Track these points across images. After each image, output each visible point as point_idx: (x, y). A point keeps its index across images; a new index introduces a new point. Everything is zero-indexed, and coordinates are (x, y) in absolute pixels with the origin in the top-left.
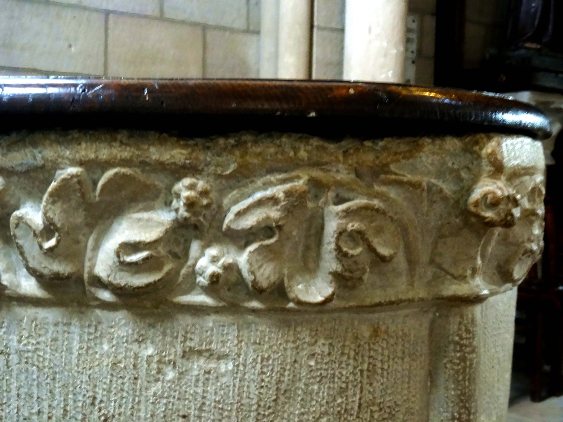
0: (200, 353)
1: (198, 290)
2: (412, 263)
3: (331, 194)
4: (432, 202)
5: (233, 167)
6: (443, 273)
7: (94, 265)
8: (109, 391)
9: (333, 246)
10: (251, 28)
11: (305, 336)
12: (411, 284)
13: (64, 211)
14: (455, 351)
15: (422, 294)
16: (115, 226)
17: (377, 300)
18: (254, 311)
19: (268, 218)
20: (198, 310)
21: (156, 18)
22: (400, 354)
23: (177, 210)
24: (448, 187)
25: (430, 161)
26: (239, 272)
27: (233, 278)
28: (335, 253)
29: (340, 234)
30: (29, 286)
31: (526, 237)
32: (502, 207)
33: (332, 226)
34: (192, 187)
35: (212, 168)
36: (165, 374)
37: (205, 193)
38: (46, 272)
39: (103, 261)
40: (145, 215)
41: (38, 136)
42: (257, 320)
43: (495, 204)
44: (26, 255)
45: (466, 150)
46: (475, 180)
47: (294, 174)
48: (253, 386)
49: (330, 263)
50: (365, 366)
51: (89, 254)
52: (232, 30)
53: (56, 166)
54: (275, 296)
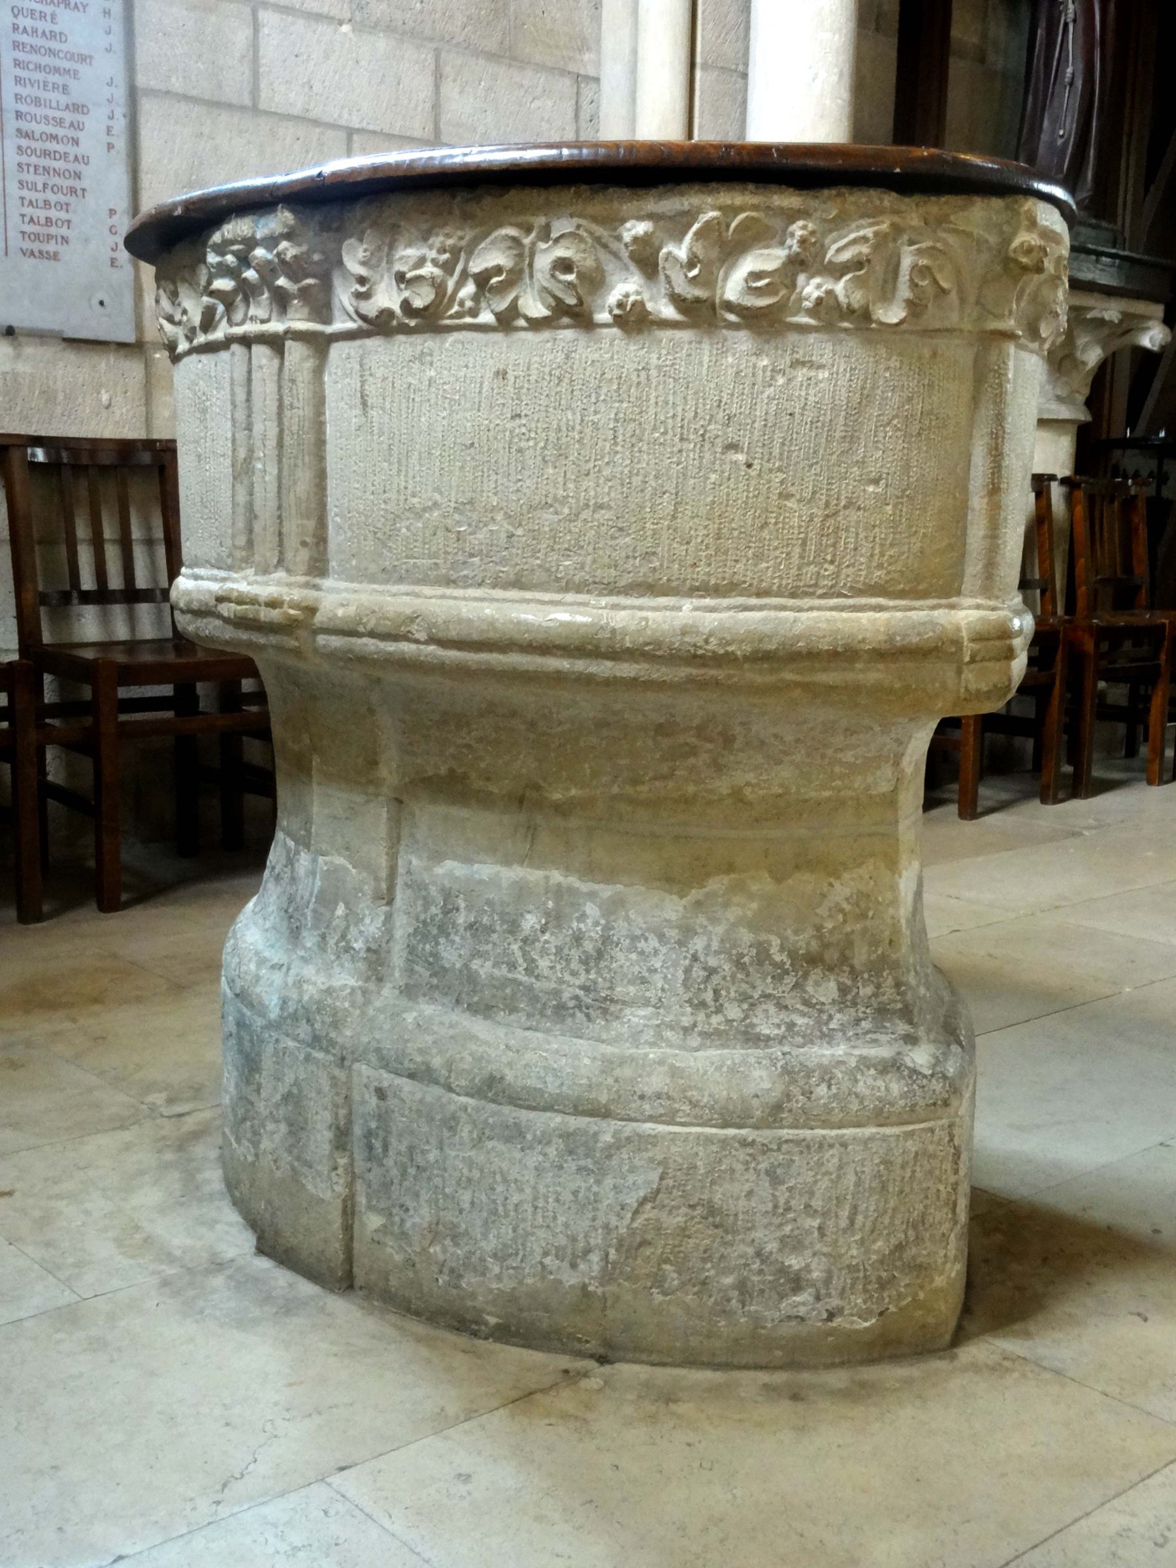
0: (803, 364)
1: (803, 313)
2: (962, 300)
3: (906, 237)
4: (979, 251)
5: (834, 213)
6: (985, 311)
7: (723, 293)
8: (732, 395)
9: (908, 277)
11: (883, 351)
12: (962, 319)
13: (704, 247)
14: (994, 377)
16: (741, 261)
18: (846, 330)
19: (860, 253)
20: (803, 329)
23: (790, 247)
24: (993, 239)
25: (978, 215)
26: (836, 297)
27: (832, 302)
28: (908, 284)
29: (913, 268)
31: (1052, 298)
32: (1035, 254)
33: (907, 262)
34: (804, 228)
35: (818, 214)
37: (813, 233)
38: (689, 296)
40: (766, 251)
41: (683, 187)
42: (848, 338)
43: (1029, 250)
44: (673, 283)
45: (1007, 208)
46: (1014, 234)
47: (880, 219)
48: (843, 390)
49: (904, 291)
50: (926, 382)
53: (699, 211)
54: (862, 317)
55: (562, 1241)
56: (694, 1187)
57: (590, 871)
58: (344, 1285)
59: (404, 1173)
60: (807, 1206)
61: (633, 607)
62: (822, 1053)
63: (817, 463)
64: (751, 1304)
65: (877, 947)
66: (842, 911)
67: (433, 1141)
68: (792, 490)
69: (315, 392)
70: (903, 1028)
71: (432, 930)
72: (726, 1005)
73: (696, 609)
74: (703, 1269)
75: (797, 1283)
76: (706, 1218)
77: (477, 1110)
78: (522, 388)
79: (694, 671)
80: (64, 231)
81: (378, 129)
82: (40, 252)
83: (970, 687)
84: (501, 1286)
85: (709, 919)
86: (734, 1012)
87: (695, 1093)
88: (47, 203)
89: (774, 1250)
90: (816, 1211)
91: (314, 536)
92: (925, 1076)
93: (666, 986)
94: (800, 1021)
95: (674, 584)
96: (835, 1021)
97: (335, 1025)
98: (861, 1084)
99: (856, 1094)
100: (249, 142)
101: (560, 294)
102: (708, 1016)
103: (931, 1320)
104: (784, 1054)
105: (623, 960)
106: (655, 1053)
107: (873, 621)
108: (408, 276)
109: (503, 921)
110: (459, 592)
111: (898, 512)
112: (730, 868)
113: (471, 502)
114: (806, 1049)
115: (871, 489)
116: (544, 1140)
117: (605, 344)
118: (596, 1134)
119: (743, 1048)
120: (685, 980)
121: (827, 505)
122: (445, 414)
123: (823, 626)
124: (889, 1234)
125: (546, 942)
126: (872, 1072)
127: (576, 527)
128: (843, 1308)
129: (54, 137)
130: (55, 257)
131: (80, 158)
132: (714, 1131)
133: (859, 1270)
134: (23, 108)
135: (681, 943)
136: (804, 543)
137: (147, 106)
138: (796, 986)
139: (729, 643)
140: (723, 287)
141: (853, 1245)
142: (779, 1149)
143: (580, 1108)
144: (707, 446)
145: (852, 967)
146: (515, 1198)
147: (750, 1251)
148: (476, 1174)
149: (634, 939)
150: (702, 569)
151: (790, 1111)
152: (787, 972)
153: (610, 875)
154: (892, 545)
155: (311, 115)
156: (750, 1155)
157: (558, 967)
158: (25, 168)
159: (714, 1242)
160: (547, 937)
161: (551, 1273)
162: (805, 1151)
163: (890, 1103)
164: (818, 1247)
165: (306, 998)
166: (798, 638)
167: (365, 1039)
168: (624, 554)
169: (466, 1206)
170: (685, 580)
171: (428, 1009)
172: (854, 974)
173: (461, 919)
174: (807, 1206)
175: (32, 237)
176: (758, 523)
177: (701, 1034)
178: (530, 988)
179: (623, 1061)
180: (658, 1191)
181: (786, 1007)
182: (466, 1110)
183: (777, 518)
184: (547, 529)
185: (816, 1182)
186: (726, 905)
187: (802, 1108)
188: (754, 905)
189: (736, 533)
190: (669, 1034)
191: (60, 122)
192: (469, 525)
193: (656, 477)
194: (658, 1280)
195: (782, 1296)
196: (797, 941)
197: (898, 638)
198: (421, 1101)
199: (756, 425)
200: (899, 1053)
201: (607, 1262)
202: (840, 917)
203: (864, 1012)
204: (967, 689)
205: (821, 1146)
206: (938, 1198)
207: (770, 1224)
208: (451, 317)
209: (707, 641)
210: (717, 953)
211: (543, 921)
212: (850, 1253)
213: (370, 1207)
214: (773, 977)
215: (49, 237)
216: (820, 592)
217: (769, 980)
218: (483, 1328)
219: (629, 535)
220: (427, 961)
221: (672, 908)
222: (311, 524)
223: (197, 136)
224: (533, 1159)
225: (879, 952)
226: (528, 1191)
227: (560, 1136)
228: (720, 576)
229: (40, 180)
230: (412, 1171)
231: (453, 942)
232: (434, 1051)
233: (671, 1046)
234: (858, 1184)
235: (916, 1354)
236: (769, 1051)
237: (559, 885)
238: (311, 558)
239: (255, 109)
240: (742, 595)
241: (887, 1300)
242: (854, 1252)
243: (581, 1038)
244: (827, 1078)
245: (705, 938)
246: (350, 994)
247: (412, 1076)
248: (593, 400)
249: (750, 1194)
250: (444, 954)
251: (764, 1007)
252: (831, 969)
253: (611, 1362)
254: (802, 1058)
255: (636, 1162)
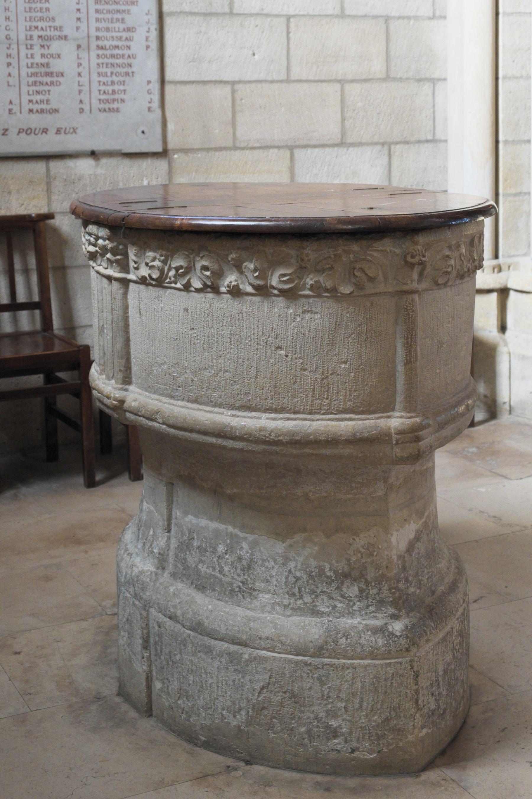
0: (308, 311)
7: (270, 282)
8: (278, 325)
10: (438, 13)
14: (405, 311)
15: (391, 290)
17: (371, 292)
18: (326, 297)
20: (307, 297)
21: (337, 16)
22: (382, 312)
30: (249, 289)
36: (296, 319)
38: (255, 284)
39: (274, 281)
50: (368, 317)
51: (269, 278)
52: (416, 18)
54: (333, 291)
55: (229, 703)
56: (285, 683)
57: (243, 528)
58: (148, 715)
59: (168, 664)
60: (338, 697)
61: (241, 417)
62: (348, 622)
63: (317, 355)
64: (314, 742)
65: (379, 570)
66: (360, 552)
67: (178, 650)
68: (306, 367)
69: (123, 304)
70: (391, 610)
71: (185, 546)
72: (304, 595)
73: (267, 419)
74: (291, 723)
75: (335, 733)
76: (291, 699)
77: (193, 637)
78: (194, 317)
79: (267, 447)
80: (122, 96)
81: (305, 13)
82: (109, 109)
83: (397, 455)
84: (205, 722)
85: (296, 554)
86: (308, 599)
87: (284, 638)
88: (113, 83)
89: (324, 717)
90: (342, 699)
91: (125, 367)
92: (397, 636)
93: (277, 584)
94: (339, 605)
95: (258, 407)
96: (356, 606)
97: (142, 589)
98: (363, 639)
99: (359, 643)
100: (228, 32)
101: (205, 280)
102: (296, 600)
103: (407, 757)
104: (328, 621)
105: (259, 570)
106: (270, 617)
107: (346, 425)
108: (150, 264)
109: (211, 547)
110: (175, 402)
111: (357, 376)
112: (304, 530)
113: (178, 363)
114: (340, 619)
115: (343, 366)
116: (220, 655)
117: (225, 302)
118: (241, 654)
119: (310, 617)
120: (286, 582)
121: (323, 373)
122: (167, 324)
123: (322, 429)
124: (381, 713)
125: (227, 559)
126: (369, 633)
127: (217, 379)
128: (359, 747)
129: (117, 47)
130: (118, 110)
131: (131, 56)
132: (292, 657)
133: (366, 730)
134: (100, 34)
135: (284, 564)
136: (314, 390)
137: (168, 21)
138: (338, 588)
139: (279, 436)
140: (271, 279)
141: (362, 717)
142: (323, 668)
143: (235, 641)
144: (268, 347)
145: (366, 580)
146: (210, 681)
147: (312, 716)
148: (194, 668)
149: (263, 560)
150: (269, 401)
151: (327, 650)
152: (333, 581)
153: (252, 531)
154: (355, 391)
155: (265, 12)
156: (309, 670)
157: (232, 571)
158: (101, 65)
159: (295, 710)
160: (227, 556)
161: (225, 718)
162: (335, 670)
163: (377, 649)
164: (345, 716)
165: (133, 574)
166: (310, 434)
167: (154, 598)
168: (236, 393)
169: (191, 682)
170: (262, 405)
171: (180, 585)
172: (367, 583)
173: (196, 543)
174: (338, 697)
175: (105, 101)
176: (292, 382)
177: (292, 609)
178: (221, 580)
179: (255, 620)
180: (269, 684)
181: (333, 598)
182: (190, 637)
183: (301, 379)
184: (206, 379)
185: (342, 684)
186: (304, 547)
187: (333, 649)
188: (316, 548)
189: (283, 386)
190: (277, 608)
191: (120, 39)
192: (177, 373)
193: (248, 360)
194: (271, 727)
195: (328, 739)
196: (338, 566)
197: (358, 434)
198: (173, 631)
199: (289, 339)
200: (386, 624)
201: (249, 716)
202: (359, 555)
203: (372, 602)
204: (396, 456)
205: (343, 668)
206: (407, 696)
207: (320, 704)
208: (167, 283)
209: (270, 435)
210: (300, 570)
211: (226, 549)
212: (361, 721)
213: (157, 678)
214: (326, 583)
215: (114, 100)
216: (323, 412)
217: (324, 584)
218: (199, 742)
219: (238, 384)
220: (182, 562)
221: (279, 548)
222: (123, 361)
223: (198, 33)
224: (216, 664)
225: (380, 573)
226: (215, 678)
227: (227, 654)
228: (277, 404)
229: (109, 71)
230: (171, 663)
231: (192, 554)
232: (179, 607)
233: (277, 614)
234: (362, 687)
235: (400, 773)
236: (322, 619)
237: (231, 533)
238: (124, 377)
239: (231, 14)
240: (288, 413)
241: (382, 745)
242: (363, 721)
243: (240, 606)
244: (346, 635)
245: (295, 563)
246: (150, 575)
247: (170, 618)
248: (221, 325)
249: (311, 688)
250: (189, 560)
251: (322, 597)
252: (355, 580)
253: (251, 764)
254: (337, 624)
255: (259, 669)
